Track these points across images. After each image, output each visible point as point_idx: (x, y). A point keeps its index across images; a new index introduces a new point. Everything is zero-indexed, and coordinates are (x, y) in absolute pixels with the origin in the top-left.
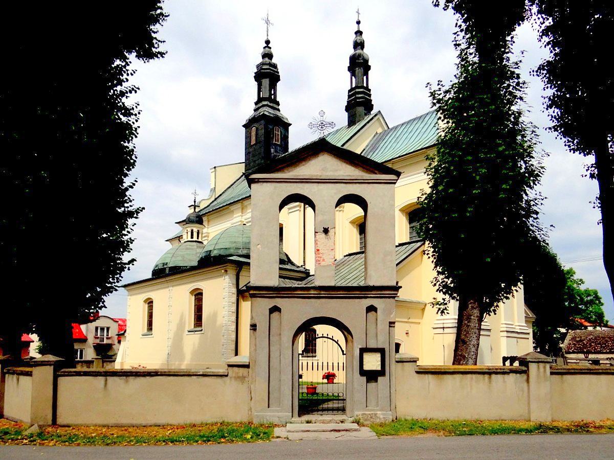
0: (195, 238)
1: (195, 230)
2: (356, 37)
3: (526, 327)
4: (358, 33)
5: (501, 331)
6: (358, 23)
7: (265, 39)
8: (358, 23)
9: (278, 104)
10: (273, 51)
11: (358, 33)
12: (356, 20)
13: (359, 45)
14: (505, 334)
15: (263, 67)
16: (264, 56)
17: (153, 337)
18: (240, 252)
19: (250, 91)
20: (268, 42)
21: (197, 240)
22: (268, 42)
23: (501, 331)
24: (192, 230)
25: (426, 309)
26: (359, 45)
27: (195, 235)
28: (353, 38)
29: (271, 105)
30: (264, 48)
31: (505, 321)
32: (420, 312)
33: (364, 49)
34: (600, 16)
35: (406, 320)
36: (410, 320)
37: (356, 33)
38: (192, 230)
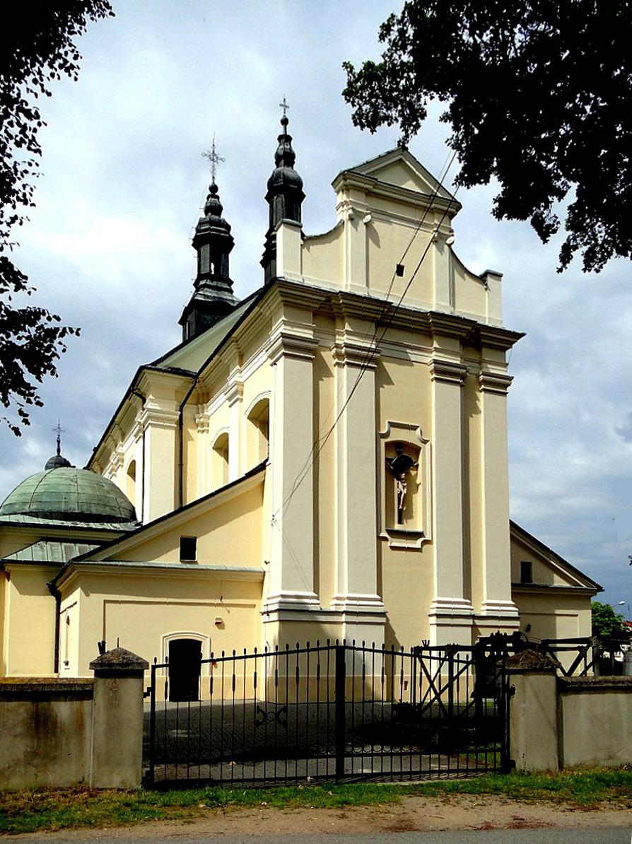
2: (280, 145)
3: (514, 606)
4: (285, 139)
5: (430, 616)
6: (285, 122)
7: (210, 183)
8: (285, 122)
9: (230, 283)
10: (222, 202)
11: (285, 139)
12: (281, 117)
13: (286, 158)
14: (433, 620)
15: (202, 228)
16: (208, 210)
17: (69, 669)
18: (27, 509)
19: (187, 262)
20: (214, 189)
22: (214, 189)
23: (430, 616)
25: (265, 581)
26: (286, 158)
28: (274, 146)
29: (214, 283)
30: (209, 196)
31: (438, 596)
32: (256, 587)
33: (294, 166)
34: (620, 69)
35: (218, 601)
36: (224, 601)
37: (280, 138)
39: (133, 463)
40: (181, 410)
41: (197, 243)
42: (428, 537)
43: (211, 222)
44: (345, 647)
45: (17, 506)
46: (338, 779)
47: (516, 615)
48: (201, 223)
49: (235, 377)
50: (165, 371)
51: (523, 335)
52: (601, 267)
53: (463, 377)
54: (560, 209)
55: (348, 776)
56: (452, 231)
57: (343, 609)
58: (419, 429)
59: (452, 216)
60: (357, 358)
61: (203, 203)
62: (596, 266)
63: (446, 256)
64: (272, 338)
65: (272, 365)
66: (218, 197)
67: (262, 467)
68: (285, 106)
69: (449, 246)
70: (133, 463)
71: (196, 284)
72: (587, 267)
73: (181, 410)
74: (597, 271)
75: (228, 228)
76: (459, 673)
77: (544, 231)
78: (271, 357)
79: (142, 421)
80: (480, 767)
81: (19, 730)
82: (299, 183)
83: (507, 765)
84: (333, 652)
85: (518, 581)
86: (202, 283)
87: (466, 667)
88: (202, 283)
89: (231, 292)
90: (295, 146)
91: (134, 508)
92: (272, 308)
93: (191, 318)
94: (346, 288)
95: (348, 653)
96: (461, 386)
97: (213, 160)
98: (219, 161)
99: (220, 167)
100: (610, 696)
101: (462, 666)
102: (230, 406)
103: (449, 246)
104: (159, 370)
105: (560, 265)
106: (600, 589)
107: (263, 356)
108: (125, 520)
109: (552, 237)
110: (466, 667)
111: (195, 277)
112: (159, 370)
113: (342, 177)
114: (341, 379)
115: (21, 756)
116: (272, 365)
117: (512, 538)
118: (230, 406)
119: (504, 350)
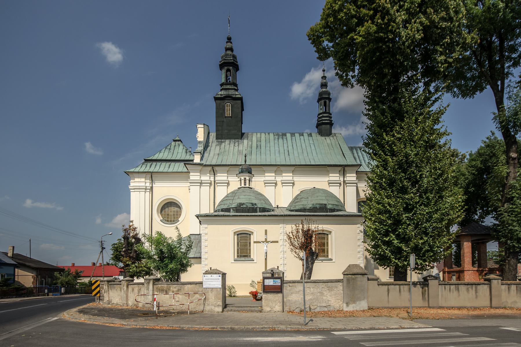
0: (243, 185)
1: (242, 178)
20: (229, 39)
21: (241, 187)
22: (229, 39)
24: (245, 179)
27: (243, 182)
38: (245, 179)
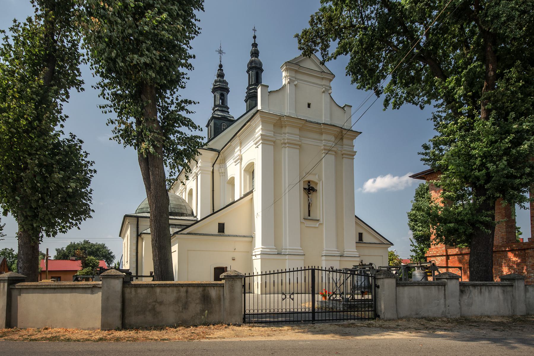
3: (357, 252)
6: (255, 37)
8: (255, 37)
9: (228, 108)
11: (255, 45)
20: (221, 66)
22: (221, 66)
28: (250, 48)
30: (219, 70)
39: (191, 190)
40: (213, 167)
41: (214, 90)
42: (322, 222)
43: (220, 81)
44: (315, 269)
45: (144, 209)
46: (313, 321)
47: (358, 256)
48: (216, 82)
49: (237, 152)
50: (206, 149)
51: (361, 133)
52: (399, 107)
53: (300, 146)
54: (385, 83)
55: (317, 320)
56: (331, 87)
57: (287, 253)
58: (317, 175)
59: (331, 80)
60: (292, 144)
61: (216, 72)
62: (397, 107)
63: (328, 99)
64: (256, 136)
65: (256, 148)
66: (222, 70)
67: (251, 192)
68: (255, 30)
69: (330, 94)
70: (191, 190)
71: (213, 110)
72: (394, 107)
73: (213, 167)
74: (398, 109)
75: (227, 84)
76: (348, 278)
77: (378, 93)
78: (255, 144)
79: (197, 172)
80: (348, 318)
81: (198, 301)
82: (261, 64)
83: (376, 316)
84: (311, 271)
85: (358, 241)
86: (217, 108)
87: (350, 276)
88: (217, 108)
89: (228, 112)
90: (259, 48)
91: (192, 210)
92: (256, 123)
93: (212, 124)
94: (287, 114)
95: (316, 271)
96: (299, 149)
97: (220, 53)
98: (223, 54)
99: (223, 56)
100: (416, 288)
101: (349, 275)
102: (236, 165)
103: (330, 94)
104: (204, 149)
105: (384, 108)
106: (392, 244)
107: (252, 143)
108: (189, 215)
109: (381, 96)
110: (350, 276)
111: (213, 106)
112: (204, 149)
113: (285, 65)
114: (286, 154)
115: (199, 312)
116: (256, 148)
117: (356, 223)
118: (236, 165)
119: (353, 139)
